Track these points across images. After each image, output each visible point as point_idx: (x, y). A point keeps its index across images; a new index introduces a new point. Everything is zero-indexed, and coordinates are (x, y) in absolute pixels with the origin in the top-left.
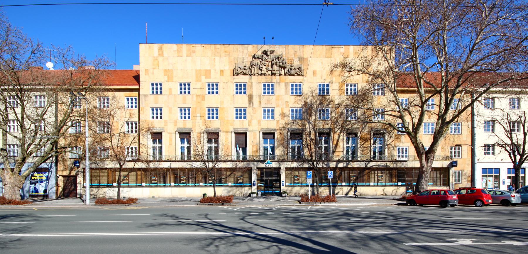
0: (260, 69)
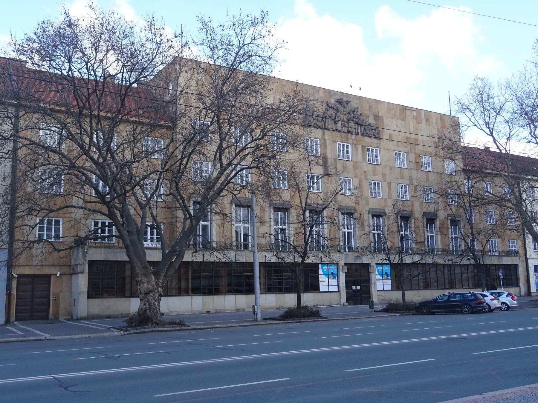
0: (335, 123)
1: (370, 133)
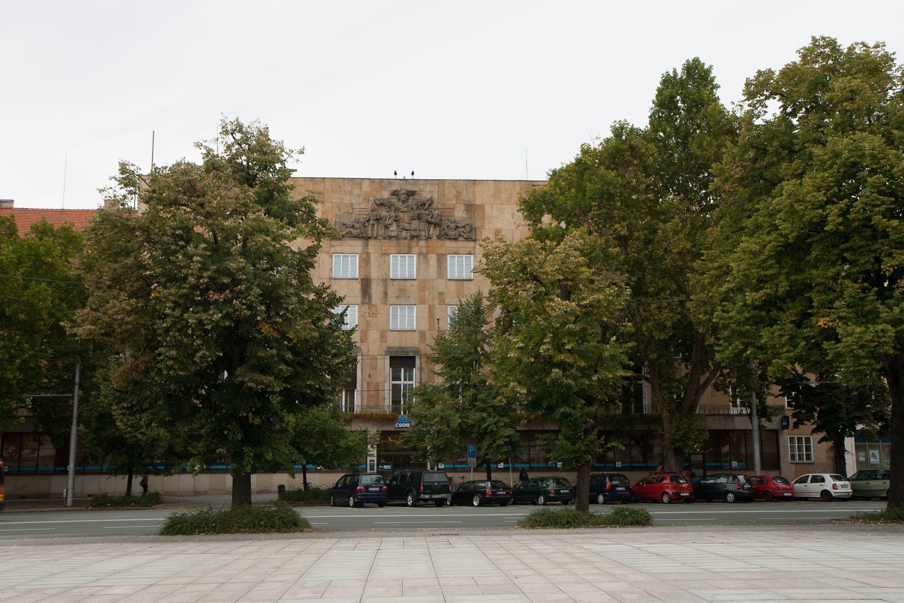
1: (452, 233)
